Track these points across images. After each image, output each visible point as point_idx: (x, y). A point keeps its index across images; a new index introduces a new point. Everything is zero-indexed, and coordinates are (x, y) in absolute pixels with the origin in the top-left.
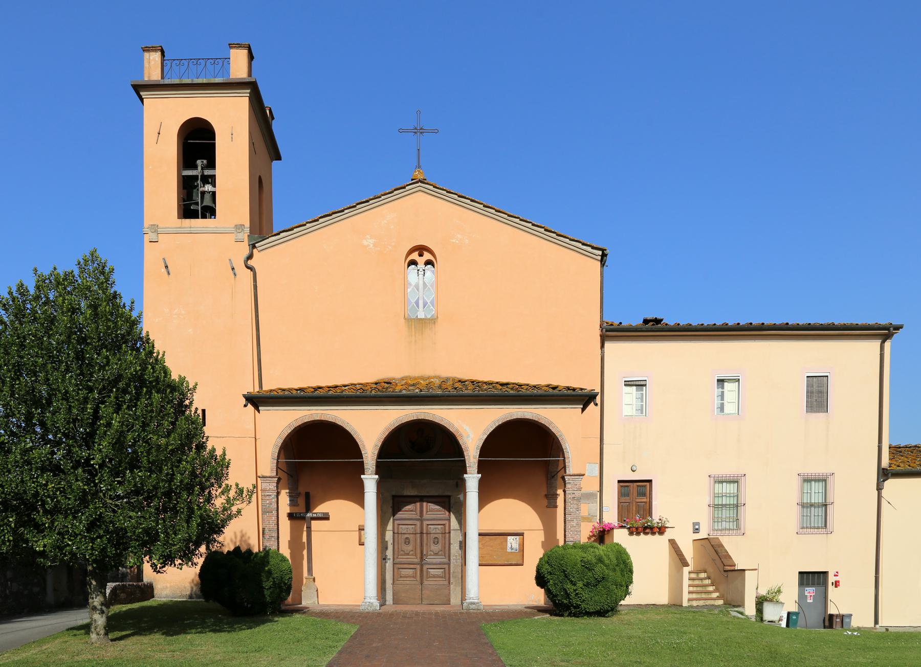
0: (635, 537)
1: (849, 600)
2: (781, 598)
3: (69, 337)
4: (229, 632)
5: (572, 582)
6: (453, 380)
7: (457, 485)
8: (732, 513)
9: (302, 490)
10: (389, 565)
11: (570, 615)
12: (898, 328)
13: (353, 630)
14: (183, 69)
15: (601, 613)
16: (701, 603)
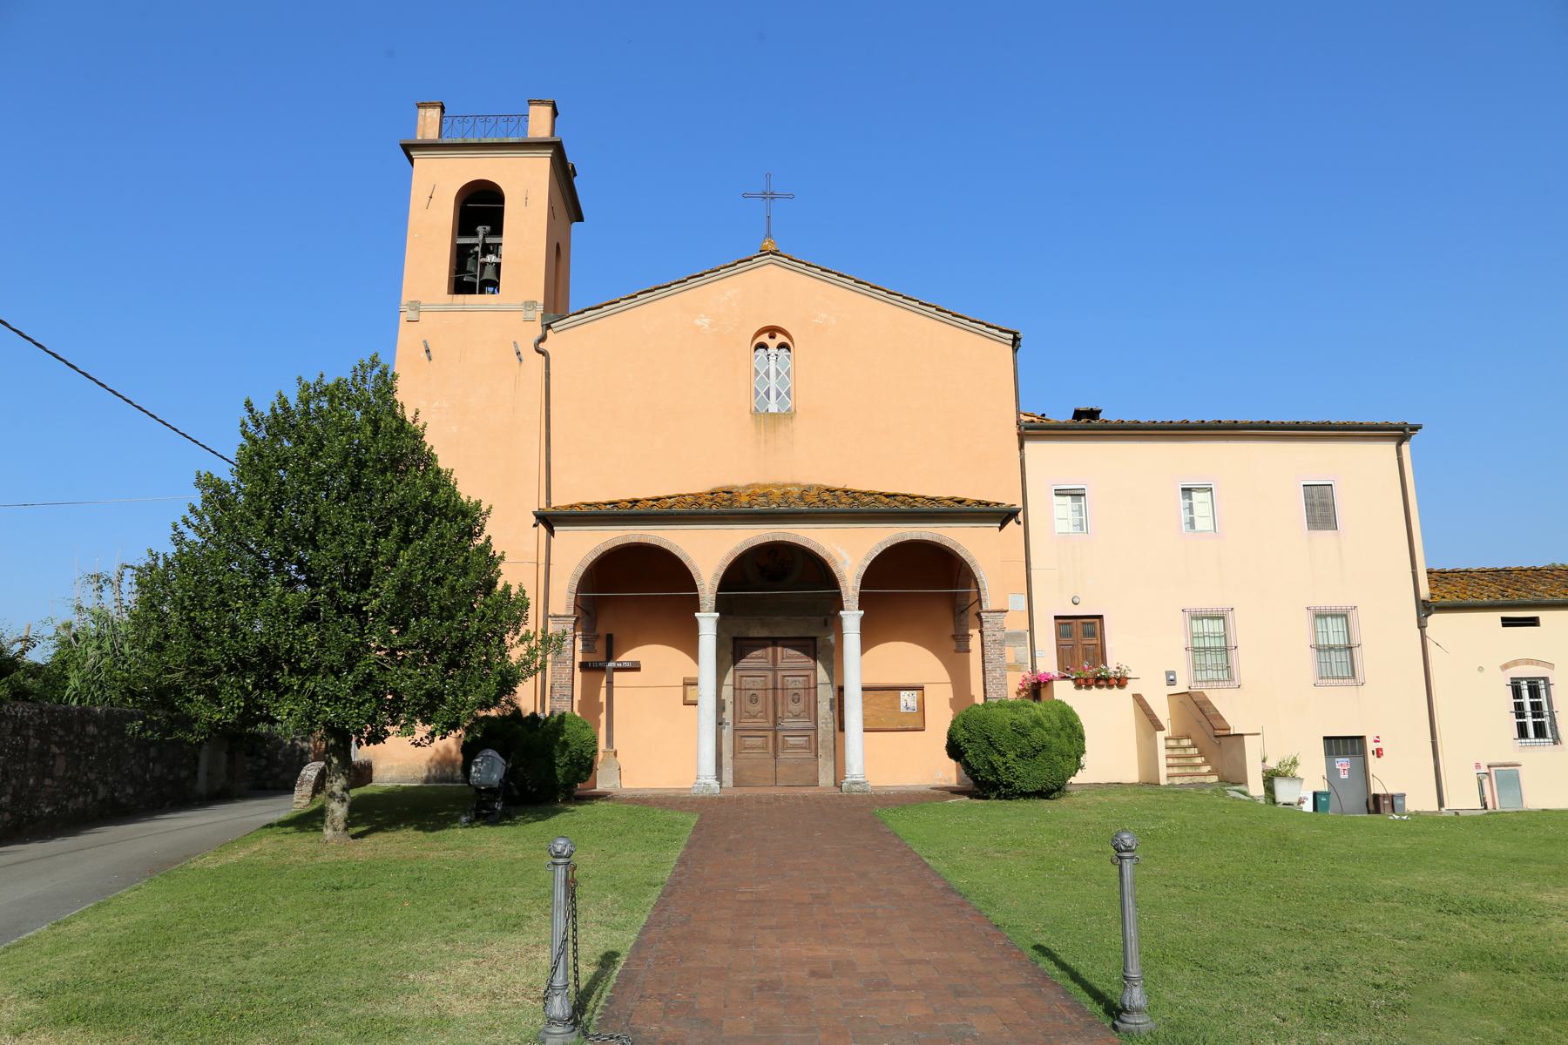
0: (1083, 691)
1: (1398, 773)
2: (1298, 772)
3: (346, 459)
6: (819, 488)
8: (1220, 659)
9: (602, 630)
10: (727, 732)
11: (998, 797)
12: (1415, 428)
13: (693, 820)
15: (1043, 794)
16: (1186, 780)
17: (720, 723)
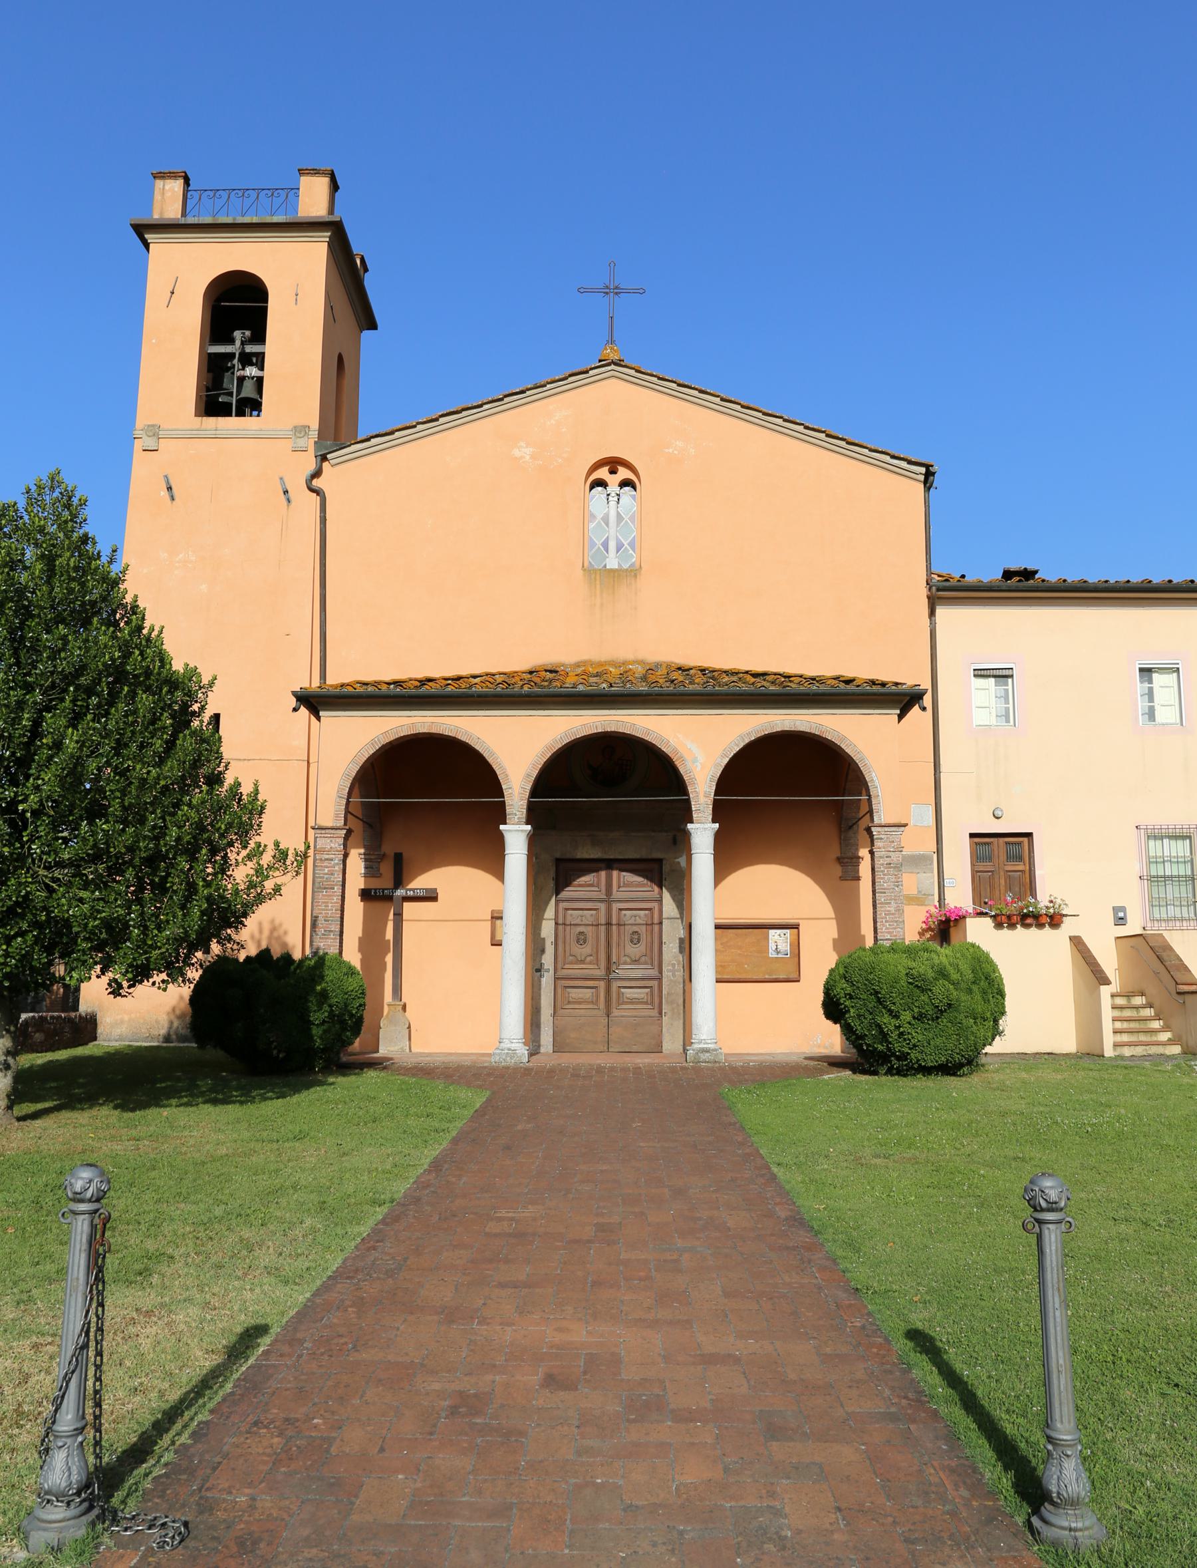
0: (1005, 932)
4: (242, 1103)
5: (890, 1011)
6: (668, 666)
7: (675, 842)
9: (389, 849)
10: (547, 980)
11: (890, 1072)
13: (479, 1099)
14: (219, 203)
15: (949, 1069)
16: (1139, 1051)
17: (535, 970)
